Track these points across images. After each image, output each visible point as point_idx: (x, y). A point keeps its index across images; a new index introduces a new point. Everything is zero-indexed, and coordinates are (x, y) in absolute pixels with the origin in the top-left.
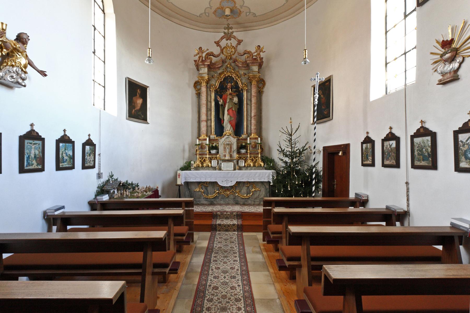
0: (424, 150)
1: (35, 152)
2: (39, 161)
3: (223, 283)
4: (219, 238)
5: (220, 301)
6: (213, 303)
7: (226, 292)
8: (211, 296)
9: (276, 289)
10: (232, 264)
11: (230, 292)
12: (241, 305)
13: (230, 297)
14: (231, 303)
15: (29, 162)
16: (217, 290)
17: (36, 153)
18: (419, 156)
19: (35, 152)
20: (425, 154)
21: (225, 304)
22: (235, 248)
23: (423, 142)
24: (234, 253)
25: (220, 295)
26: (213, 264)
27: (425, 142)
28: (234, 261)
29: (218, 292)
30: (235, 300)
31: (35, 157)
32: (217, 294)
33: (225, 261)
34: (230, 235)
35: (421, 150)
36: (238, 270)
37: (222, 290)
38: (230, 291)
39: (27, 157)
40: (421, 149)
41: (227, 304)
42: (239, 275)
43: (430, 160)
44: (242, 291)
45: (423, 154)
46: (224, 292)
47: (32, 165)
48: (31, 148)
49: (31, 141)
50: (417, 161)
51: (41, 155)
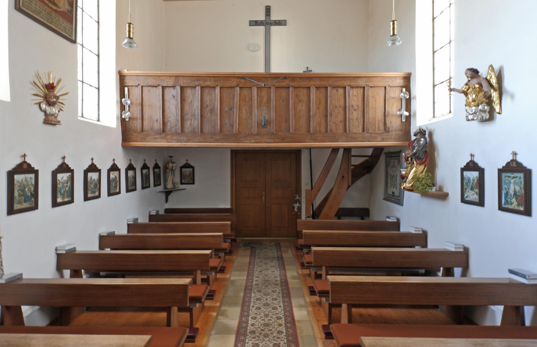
0: (27, 189)
1: (515, 188)
2: (521, 200)
3: (269, 295)
4: (275, 272)
5: (270, 332)
6: (277, 330)
7: (265, 341)
8: (280, 337)
9: (208, 341)
10: (259, 313)
11: (260, 340)
12: (250, 327)
13: (260, 335)
14: (259, 330)
15: (508, 200)
16: (274, 343)
17: (516, 189)
18: (20, 198)
19: (515, 188)
20: (28, 194)
21: (265, 329)
22: (258, 261)
23: (26, 180)
24: (258, 284)
25: (271, 337)
26: (281, 314)
27: (28, 181)
28: (258, 277)
29: (273, 341)
30: (256, 332)
31: (515, 194)
32: (274, 339)
33: (267, 277)
34: (262, 275)
35: (23, 190)
36: (253, 307)
37: (268, 343)
38: (260, 342)
39: (504, 193)
40: (23, 188)
41: (263, 328)
42: (252, 301)
43: (33, 200)
44: (247, 341)
45: (26, 194)
46: (266, 341)
47: (512, 204)
48: (510, 183)
49: (509, 174)
50: (17, 204)
51: (523, 192)
